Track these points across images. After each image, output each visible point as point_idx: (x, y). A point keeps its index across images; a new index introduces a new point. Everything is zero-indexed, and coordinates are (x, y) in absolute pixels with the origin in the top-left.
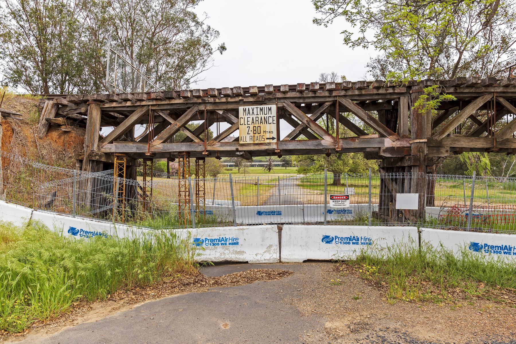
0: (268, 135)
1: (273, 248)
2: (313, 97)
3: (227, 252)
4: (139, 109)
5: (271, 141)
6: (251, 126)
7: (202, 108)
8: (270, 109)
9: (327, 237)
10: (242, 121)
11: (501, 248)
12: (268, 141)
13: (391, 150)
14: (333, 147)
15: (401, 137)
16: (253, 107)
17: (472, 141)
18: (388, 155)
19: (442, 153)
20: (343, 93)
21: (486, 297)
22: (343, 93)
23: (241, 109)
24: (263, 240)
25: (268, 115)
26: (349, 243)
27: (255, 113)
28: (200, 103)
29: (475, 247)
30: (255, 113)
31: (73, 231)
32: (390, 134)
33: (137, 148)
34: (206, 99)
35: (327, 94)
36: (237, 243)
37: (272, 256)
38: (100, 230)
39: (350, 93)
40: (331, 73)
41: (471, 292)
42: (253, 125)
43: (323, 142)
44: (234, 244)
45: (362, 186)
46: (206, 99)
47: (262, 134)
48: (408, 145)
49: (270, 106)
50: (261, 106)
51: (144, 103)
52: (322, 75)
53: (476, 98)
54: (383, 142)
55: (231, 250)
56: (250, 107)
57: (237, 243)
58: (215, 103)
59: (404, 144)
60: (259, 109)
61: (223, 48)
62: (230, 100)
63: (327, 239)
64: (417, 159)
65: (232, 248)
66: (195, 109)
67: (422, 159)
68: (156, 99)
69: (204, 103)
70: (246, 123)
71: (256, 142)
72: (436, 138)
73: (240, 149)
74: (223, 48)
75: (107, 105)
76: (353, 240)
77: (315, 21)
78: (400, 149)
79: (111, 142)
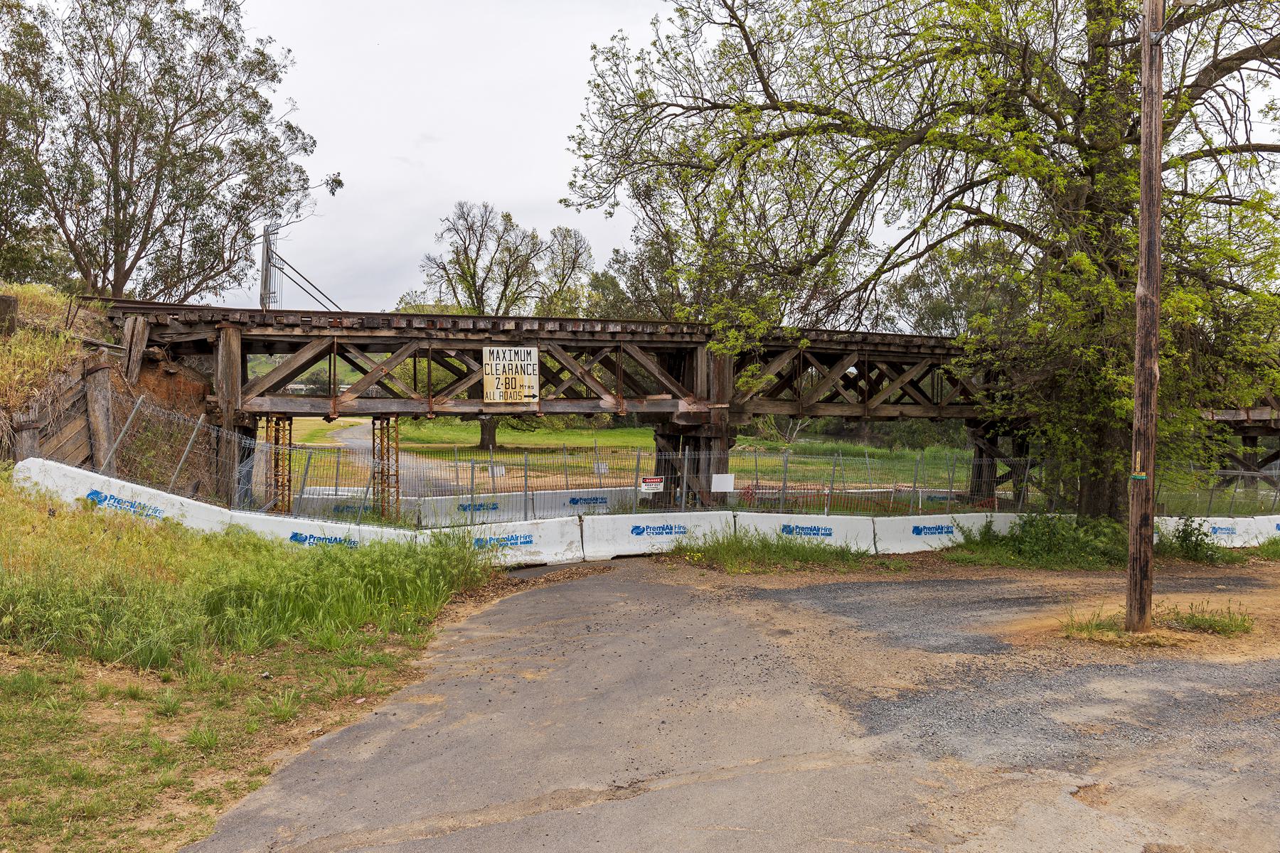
0: (527, 392)
1: (574, 546)
2: (589, 340)
3: (518, 553)
4: (315, 342)
5: (531, 400)
6: (503, 378)
7: (425, 345)
8: (529, 354)
9: (637, 528)
10: (488, 369)
11: (811, 529)
12: (526, 400)
13: (686, 415)
14: (615, 410)
15: (698, 400)
16: (504, 349)
17: (777, 406)
18: (683, 423)
19: (744, 421)
20: (629, 338)
21: (802, 569)
22: (629, 338)
23: (486, 350)
24: (562, 535)
25: (526, 362)
26: (662, 533)
27: (508, 358)
28: (423, 339)
29: (787, 529)
30: (508, 358)
31: (295, 537)
32: (685, 395)
33: (312, 406)
34: (433, 332)
35: (609, 338)
36: (531, 542)
37: (573, 555)
38: (340, 535)
39: (638, 338)
40: (480, 203)
41: (790, 566)
42: (504, 376)
43: (602, 403)
44: (527, 542)
45: (277, 431)
46: (433, 332)
47: (518, 390)
48: (706, 410)
49: (529, 349)
50: (516, 349)
51: (326, 333)
52: (461, 206)
53: (782, 352)
54: (676, 406)
55: (524, 550)
56: (500, 349)
57: (531, 542)
58: (447, 340)
59: (702, 408)
60: (513, 353)
61: (336, 183)
62: (470, 336)
63: (637, 531)
64: (719, 429)
65: (524, 548)
66: (414, 346)
67: (724, 429)
68: (347, 328)
69: (430, 338)
70: (494, 372)
71: (509, 401)
72: (738, 401)
73: (485, 410)
74: (336, 183)
75: (255, 332)
76: (667, 529)
77: (565, 202)
78: (696, 415)
79: (262, 395)
